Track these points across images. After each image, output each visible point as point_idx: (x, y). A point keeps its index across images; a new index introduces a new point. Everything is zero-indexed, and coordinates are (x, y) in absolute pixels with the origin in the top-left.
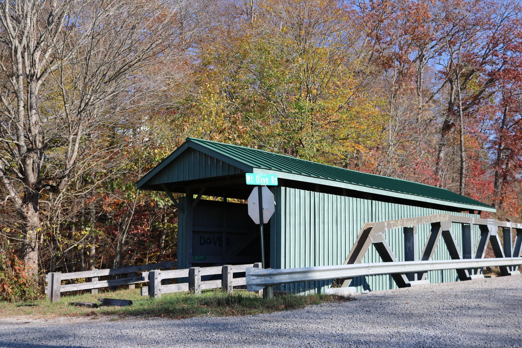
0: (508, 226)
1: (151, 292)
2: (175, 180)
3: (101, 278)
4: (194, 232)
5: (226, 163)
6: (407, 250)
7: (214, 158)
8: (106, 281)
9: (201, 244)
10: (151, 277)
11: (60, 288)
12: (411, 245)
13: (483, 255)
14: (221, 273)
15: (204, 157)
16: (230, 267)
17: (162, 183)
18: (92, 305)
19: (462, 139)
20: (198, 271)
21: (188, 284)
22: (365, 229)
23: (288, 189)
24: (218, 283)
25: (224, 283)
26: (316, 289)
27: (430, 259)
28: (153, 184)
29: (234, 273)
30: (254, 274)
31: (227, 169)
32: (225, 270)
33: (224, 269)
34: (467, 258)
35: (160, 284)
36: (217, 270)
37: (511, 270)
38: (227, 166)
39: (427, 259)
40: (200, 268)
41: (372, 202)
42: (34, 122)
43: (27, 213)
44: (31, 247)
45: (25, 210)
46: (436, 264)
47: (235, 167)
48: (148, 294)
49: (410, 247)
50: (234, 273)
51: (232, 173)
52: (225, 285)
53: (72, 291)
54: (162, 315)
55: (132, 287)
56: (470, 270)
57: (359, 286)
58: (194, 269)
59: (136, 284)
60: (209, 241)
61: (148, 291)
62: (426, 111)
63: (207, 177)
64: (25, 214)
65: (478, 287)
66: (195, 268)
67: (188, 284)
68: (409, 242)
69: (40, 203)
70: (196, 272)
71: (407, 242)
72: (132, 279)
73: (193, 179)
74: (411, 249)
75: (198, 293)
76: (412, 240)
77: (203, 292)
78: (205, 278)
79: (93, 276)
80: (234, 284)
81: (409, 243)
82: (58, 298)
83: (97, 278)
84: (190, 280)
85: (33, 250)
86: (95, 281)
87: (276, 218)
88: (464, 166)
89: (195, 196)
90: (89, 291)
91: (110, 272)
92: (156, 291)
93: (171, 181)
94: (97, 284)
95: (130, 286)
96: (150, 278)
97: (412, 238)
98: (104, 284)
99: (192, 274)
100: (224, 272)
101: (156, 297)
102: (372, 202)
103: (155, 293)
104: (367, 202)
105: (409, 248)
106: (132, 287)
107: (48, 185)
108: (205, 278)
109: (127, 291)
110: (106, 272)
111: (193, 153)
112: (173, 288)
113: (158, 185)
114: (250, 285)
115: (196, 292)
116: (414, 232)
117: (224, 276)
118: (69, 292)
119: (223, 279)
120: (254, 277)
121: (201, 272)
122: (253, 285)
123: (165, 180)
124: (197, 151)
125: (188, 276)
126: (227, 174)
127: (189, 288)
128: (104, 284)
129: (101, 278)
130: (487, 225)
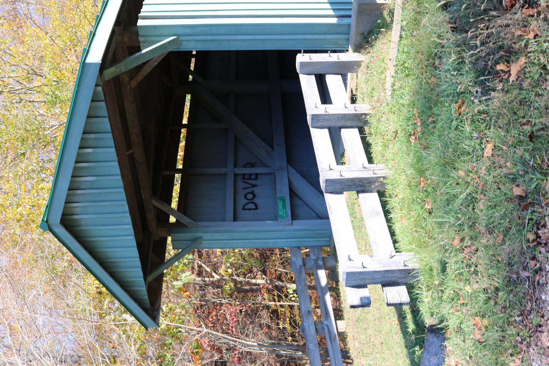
2: (135, 252)
7: (75, 169)
9: (256, 208)
17: (142, 279)
20: (331, 172)
23: (141, 14)
26: (334, 21)
28: (147, 297)
47: (89, 117)
51: (105, 124)
55: (342, 325)
58: (327, 181)
59: (336, 320)
60: (250, 196)
72: (327, 326)
73: (128, 215)
89: (172, 219)
93: (137, 262)
95: (339, 331)
96: (361, 283)
100: (325, 124)
101: (410, 266)
103: (402, 267)
106: (342, 325)
117: (332, 124)
119: (339, 124)
124: (65, 208)
126: (110, 135)
127: (371, 192)
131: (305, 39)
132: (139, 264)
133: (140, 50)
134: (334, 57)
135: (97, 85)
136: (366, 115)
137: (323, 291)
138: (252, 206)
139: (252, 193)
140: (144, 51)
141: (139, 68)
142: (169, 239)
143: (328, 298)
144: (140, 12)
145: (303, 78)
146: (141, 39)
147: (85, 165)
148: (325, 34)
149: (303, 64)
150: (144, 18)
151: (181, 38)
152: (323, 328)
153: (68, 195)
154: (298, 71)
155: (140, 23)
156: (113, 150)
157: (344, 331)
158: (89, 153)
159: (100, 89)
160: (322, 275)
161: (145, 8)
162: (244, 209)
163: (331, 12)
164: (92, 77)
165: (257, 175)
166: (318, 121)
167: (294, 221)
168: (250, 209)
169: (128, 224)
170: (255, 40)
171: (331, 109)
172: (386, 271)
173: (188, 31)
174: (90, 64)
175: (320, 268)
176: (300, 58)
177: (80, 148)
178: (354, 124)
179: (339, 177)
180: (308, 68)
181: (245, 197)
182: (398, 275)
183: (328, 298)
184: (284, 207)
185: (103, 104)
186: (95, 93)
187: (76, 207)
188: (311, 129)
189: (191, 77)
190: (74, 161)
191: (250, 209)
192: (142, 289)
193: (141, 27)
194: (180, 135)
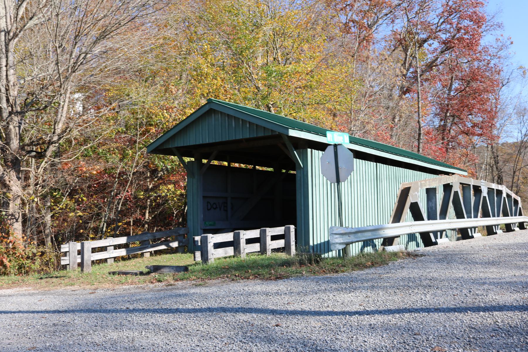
0: (493, 187)
1: (205, 257)
2: (200, 141)
3: (117, 247)
4: (204, 197)
5: (253, 124)
6: (430, 210)
7: (239, 119)
8: (124, 250)
9: (208, 210)
10: (205, 241)
11: (90, 256)
12: (433, 205)
13: (479, 215)
14: (259, 236)
15: (227, 118)
16: (242, 232)
18: (138, 273)
19: (420, 106)
21: (233, 248)
22: (402, 189)
23: (313, 150)
24: (230, 251)
25: (262, 246)
26: (311, 244)
27: (447, 218)
29: (272, 236)
30: (337, 233)
31: (255, 130)
32: (263, 233)
33: (262, 233)
34: (432, 219)
35: (213, 248)
36: (228, 237)
37: (436, 238)
38: (255, 127)
39: (399, 222)
40: (245, 231)
41: (376, 164)
42: (12, 84)
43: (9, 181)
44: (15, 218)
45: (7, 178)
46: (414, 225)
47: (264, 128)
48: (200, 259)
49: (432, 207)
50: (272, 236)
51: (261, 134)
52: (263, 250)
53: (185, 253)
54: (251, 278)
56: (435, 233)
57: (326, 253)
58: (239, 233)
60: (214, 206)
61: (200, 256)
62: (75, 94)
63: (231, 139)
64: (8, 183)
65: (481, 243)
66: (240, 231)
67: (233, 248)
68: (431, 202)
69: (22, 170)
70: (241, 236)
71: (429, 202)
73: (214, 141)
74: (434, 209)
75: (243, 256)
76: (434, 200)
77: (248, 254)
78: (218, 246)
79: (109, 245)
80: (247, 251)
81: (431, 203)
82: (89, 268)
83: (113, 247)
84: (235, 244)
85: (17, 221)
86: (110, 250)
87: (302, 181)
88: (422, 132)
89: (205, 161)
90: (105, 260)
91: (127, 239)
92: (210, 256)
94: (113, 253)
97: (434, 197)
98: (122, 252)
99: (237, 238)
101: (209, 261)
102: (376, 164)
103: (209, 258)
104: (373, 164)
105: (432, 208)
107: (33, 151)
108: (218, 246)
109: (106, 264)
110: (123, 240)
111: (213, 115)
112: (221, 252)
113: (170, 149)
114: (334, 244)
115: (242, 255)
116: (437, 192)
117: (262, 240)
118: (101, 260)
119: (262, 242)
120: (337, 236)
121: (271, 232)
122: (337, 243)
123: (180, 143)
124: (218, 111)
125: (232, 240)
127: (235, 252)
128: (122, 252)
129: (117, 247)
130: (480, 187)
131: (302, 231)
132: (185, 145)
133: (296, 149)
134: (293, 243)
135: (279, 132)
136: (266, 254)
137: (167, 245)
138: (209, 207)
139: (216, 208)
140: (295, 152)
141: (287, 148)
142: (193, 159)
143: (163, 247)
144: (314, 149)
145: (283, 228)
146: (301, 150)
147: (241, 122)
148: (305, 240)
149: (289, 228)
150: (312, 152)
151: (302, 169)
152: (146, 245)
153: (225, 114)
154: (286, 226)
155: (309, 150)
156: (248, 137)
157: (144, 256)
158: (247, 125)
159: (277, 133)
160: (175, 245)
161: (316, 151)
162: (208, 202)
163: (315, 243)
164: (281, 131)
165: (226, 211)
166: (263, 232)
167: (202, 230)
168: (207, 206)
169: (202, 141)
170: (301, 206)
171: (268, 239)
172: (208, 251)
173: (305, 173)
174: (288, 131)
175: (179, 244)
176: (292, 227)
177: (249, 122)
178: (262, 249)
179: (241, 238)
180: (287, 231)
181: (214, 203)
182: (206, 256)
183: (163, 247)
184: (211, 225)
185: (270, 134)
186: (275, 131)
187: (218, 116)
188: (259, 230)
189: (284, 171)
190: (243, 119)
191: (207, 206)
192: (170, 146)
193: (307, 150)
194: (259, 170)
